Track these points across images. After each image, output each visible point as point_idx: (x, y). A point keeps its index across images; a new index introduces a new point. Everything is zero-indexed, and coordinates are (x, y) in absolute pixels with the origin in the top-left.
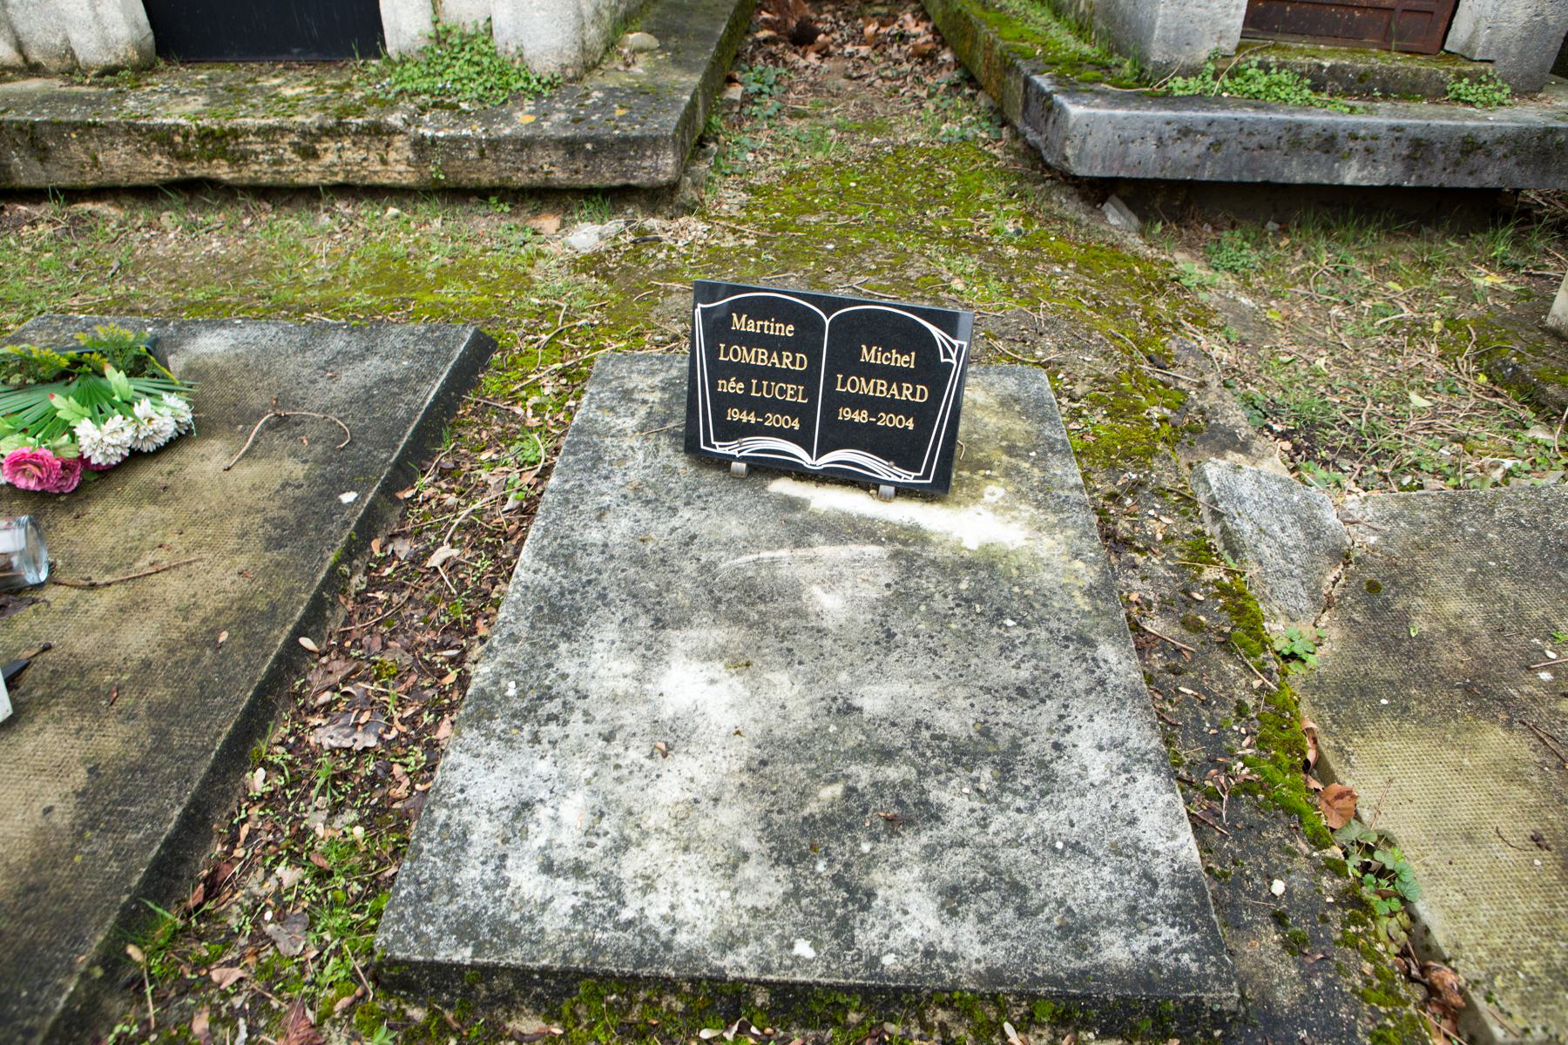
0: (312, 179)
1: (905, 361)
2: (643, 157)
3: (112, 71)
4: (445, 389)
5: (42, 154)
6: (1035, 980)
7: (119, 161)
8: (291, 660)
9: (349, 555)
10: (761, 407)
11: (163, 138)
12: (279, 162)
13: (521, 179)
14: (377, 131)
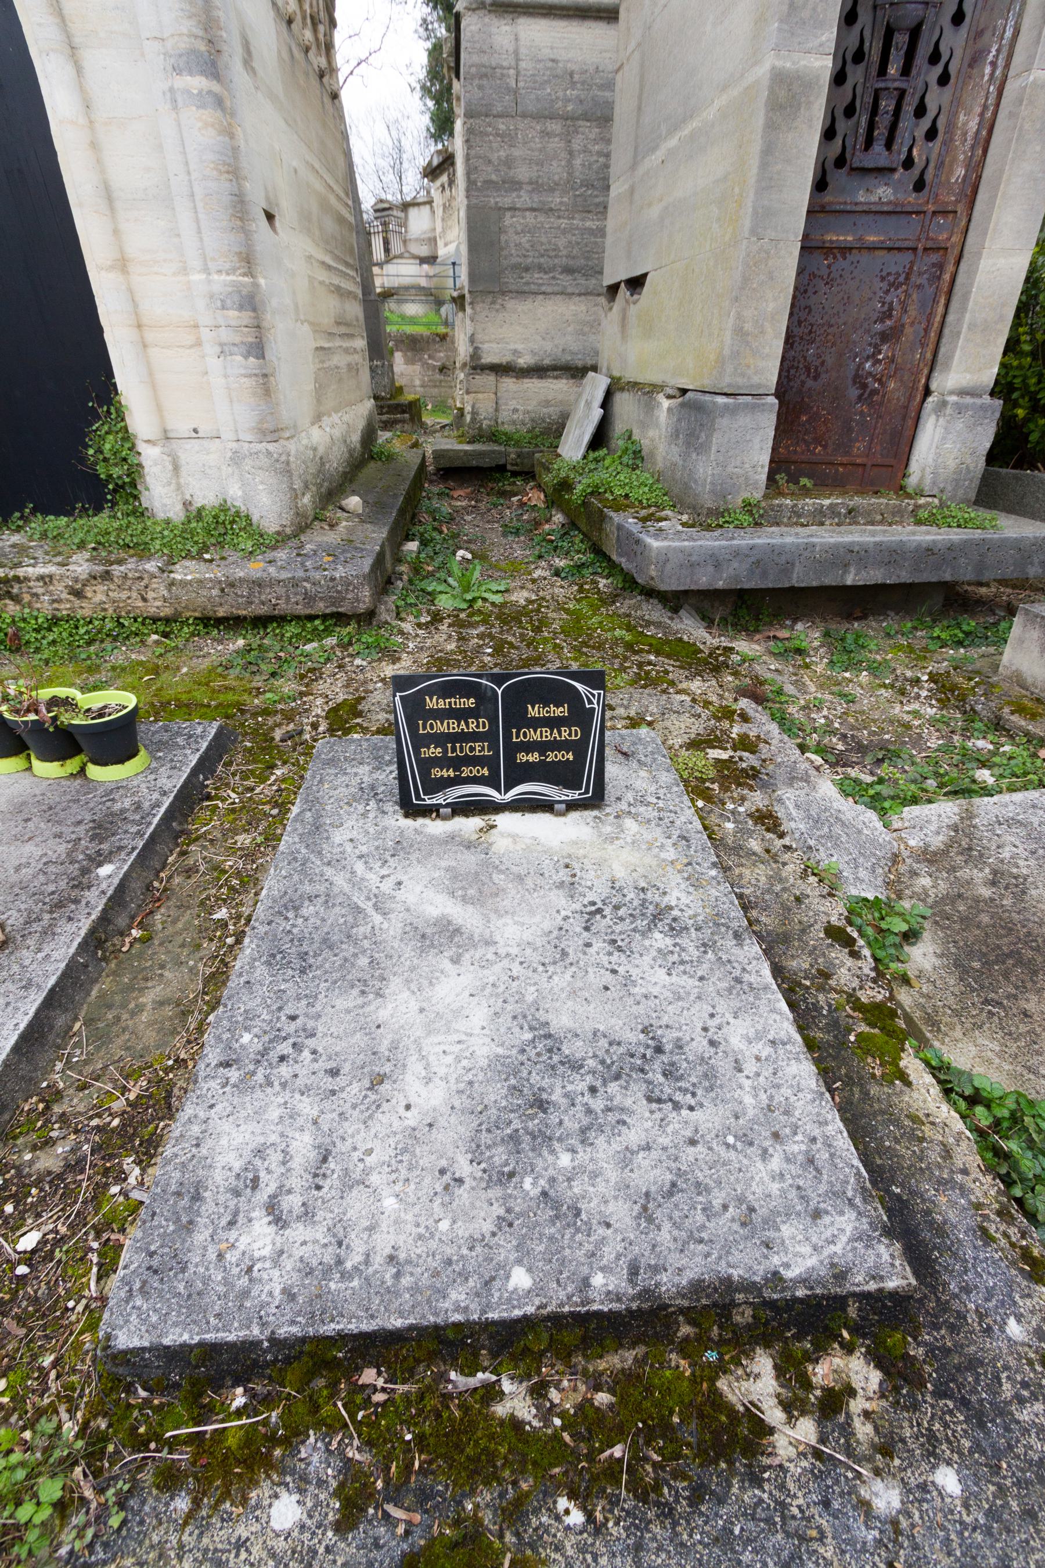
1: (560, 711)
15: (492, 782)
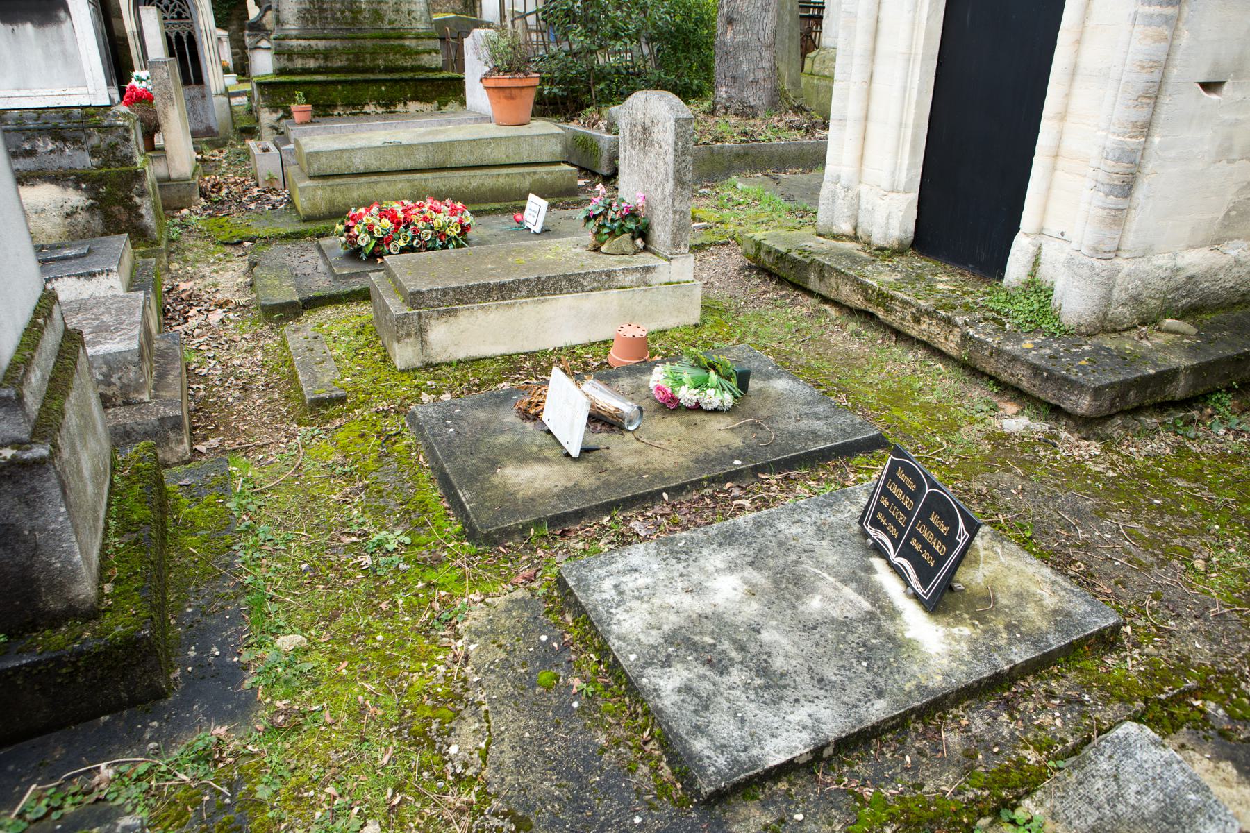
0: (914, 333)
1: (944, 530)
2: (1072, 393)
3: (882, 249)
4: (830, 449)
5: (822, 278)
6: (667, 724)
7: (846, 292)
8: (655, 497)
9: (712, 480)
10: (890, 519)
11: (864, 288)
12: (903, 319)
13: (1005, 377)
14: (949, 322)
15: (895, 542)
